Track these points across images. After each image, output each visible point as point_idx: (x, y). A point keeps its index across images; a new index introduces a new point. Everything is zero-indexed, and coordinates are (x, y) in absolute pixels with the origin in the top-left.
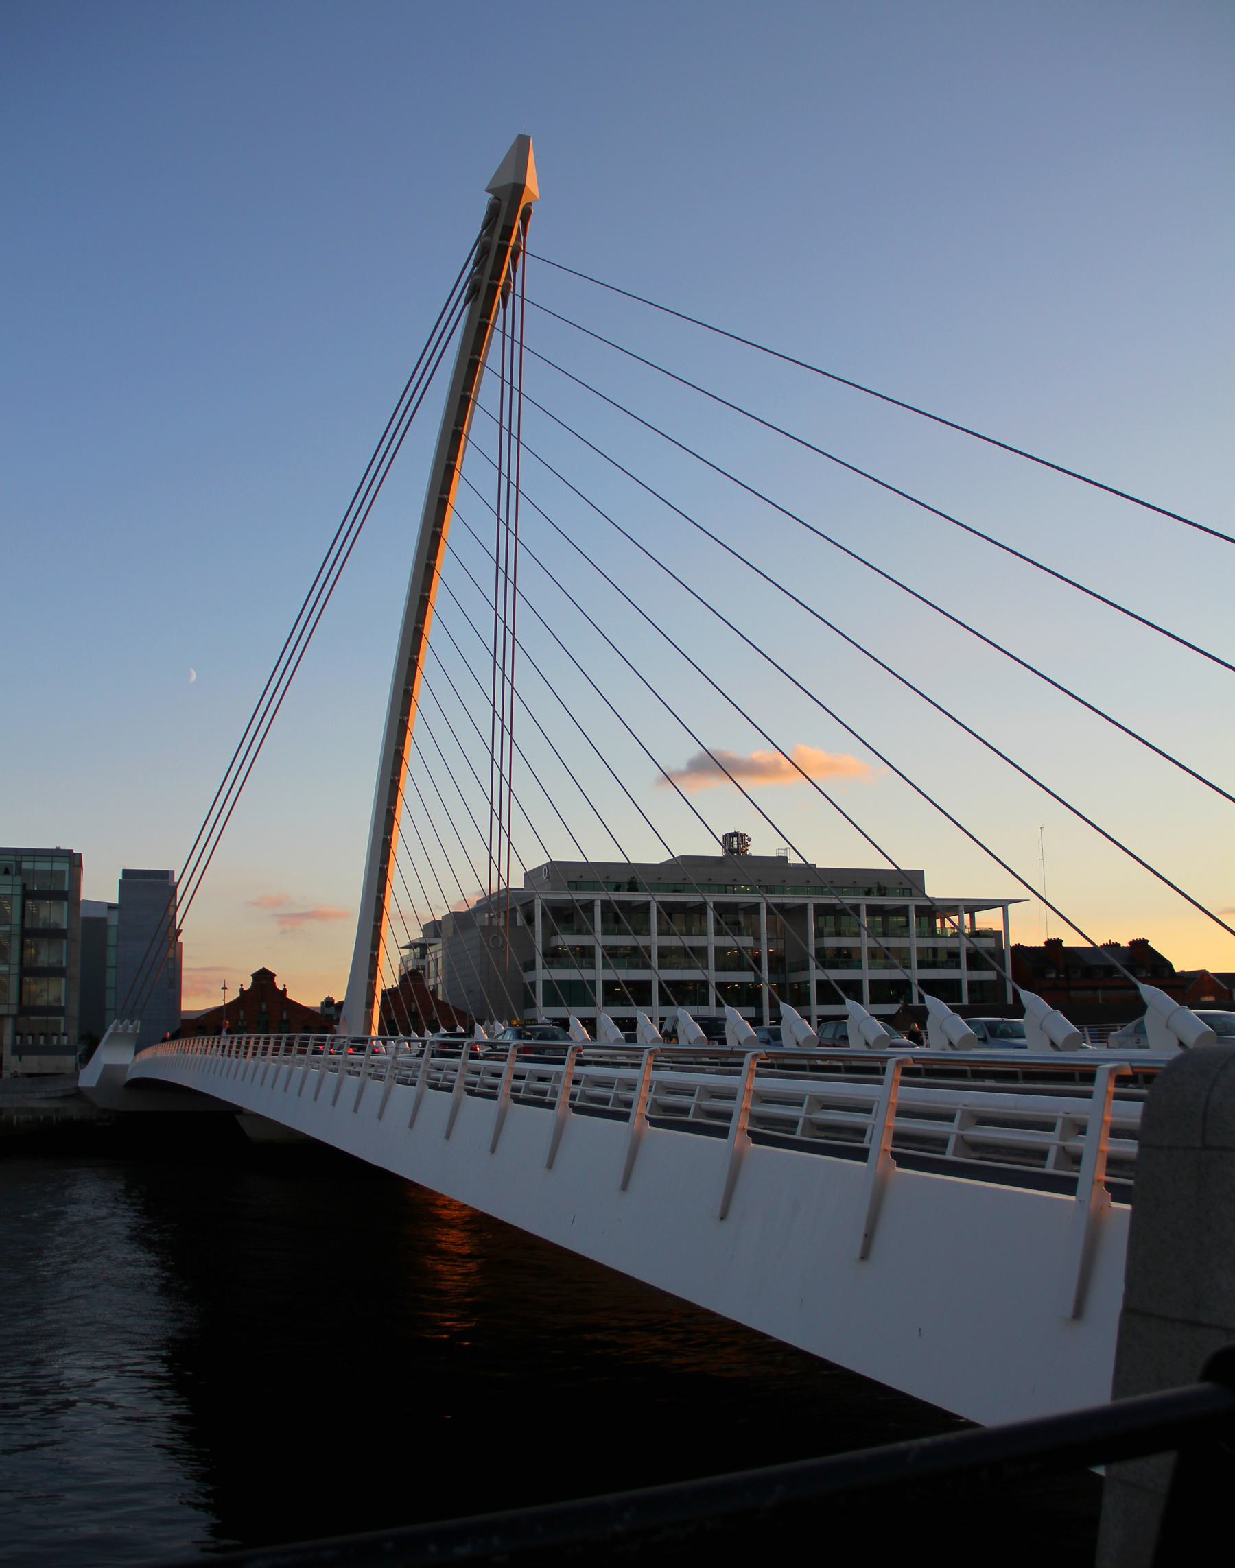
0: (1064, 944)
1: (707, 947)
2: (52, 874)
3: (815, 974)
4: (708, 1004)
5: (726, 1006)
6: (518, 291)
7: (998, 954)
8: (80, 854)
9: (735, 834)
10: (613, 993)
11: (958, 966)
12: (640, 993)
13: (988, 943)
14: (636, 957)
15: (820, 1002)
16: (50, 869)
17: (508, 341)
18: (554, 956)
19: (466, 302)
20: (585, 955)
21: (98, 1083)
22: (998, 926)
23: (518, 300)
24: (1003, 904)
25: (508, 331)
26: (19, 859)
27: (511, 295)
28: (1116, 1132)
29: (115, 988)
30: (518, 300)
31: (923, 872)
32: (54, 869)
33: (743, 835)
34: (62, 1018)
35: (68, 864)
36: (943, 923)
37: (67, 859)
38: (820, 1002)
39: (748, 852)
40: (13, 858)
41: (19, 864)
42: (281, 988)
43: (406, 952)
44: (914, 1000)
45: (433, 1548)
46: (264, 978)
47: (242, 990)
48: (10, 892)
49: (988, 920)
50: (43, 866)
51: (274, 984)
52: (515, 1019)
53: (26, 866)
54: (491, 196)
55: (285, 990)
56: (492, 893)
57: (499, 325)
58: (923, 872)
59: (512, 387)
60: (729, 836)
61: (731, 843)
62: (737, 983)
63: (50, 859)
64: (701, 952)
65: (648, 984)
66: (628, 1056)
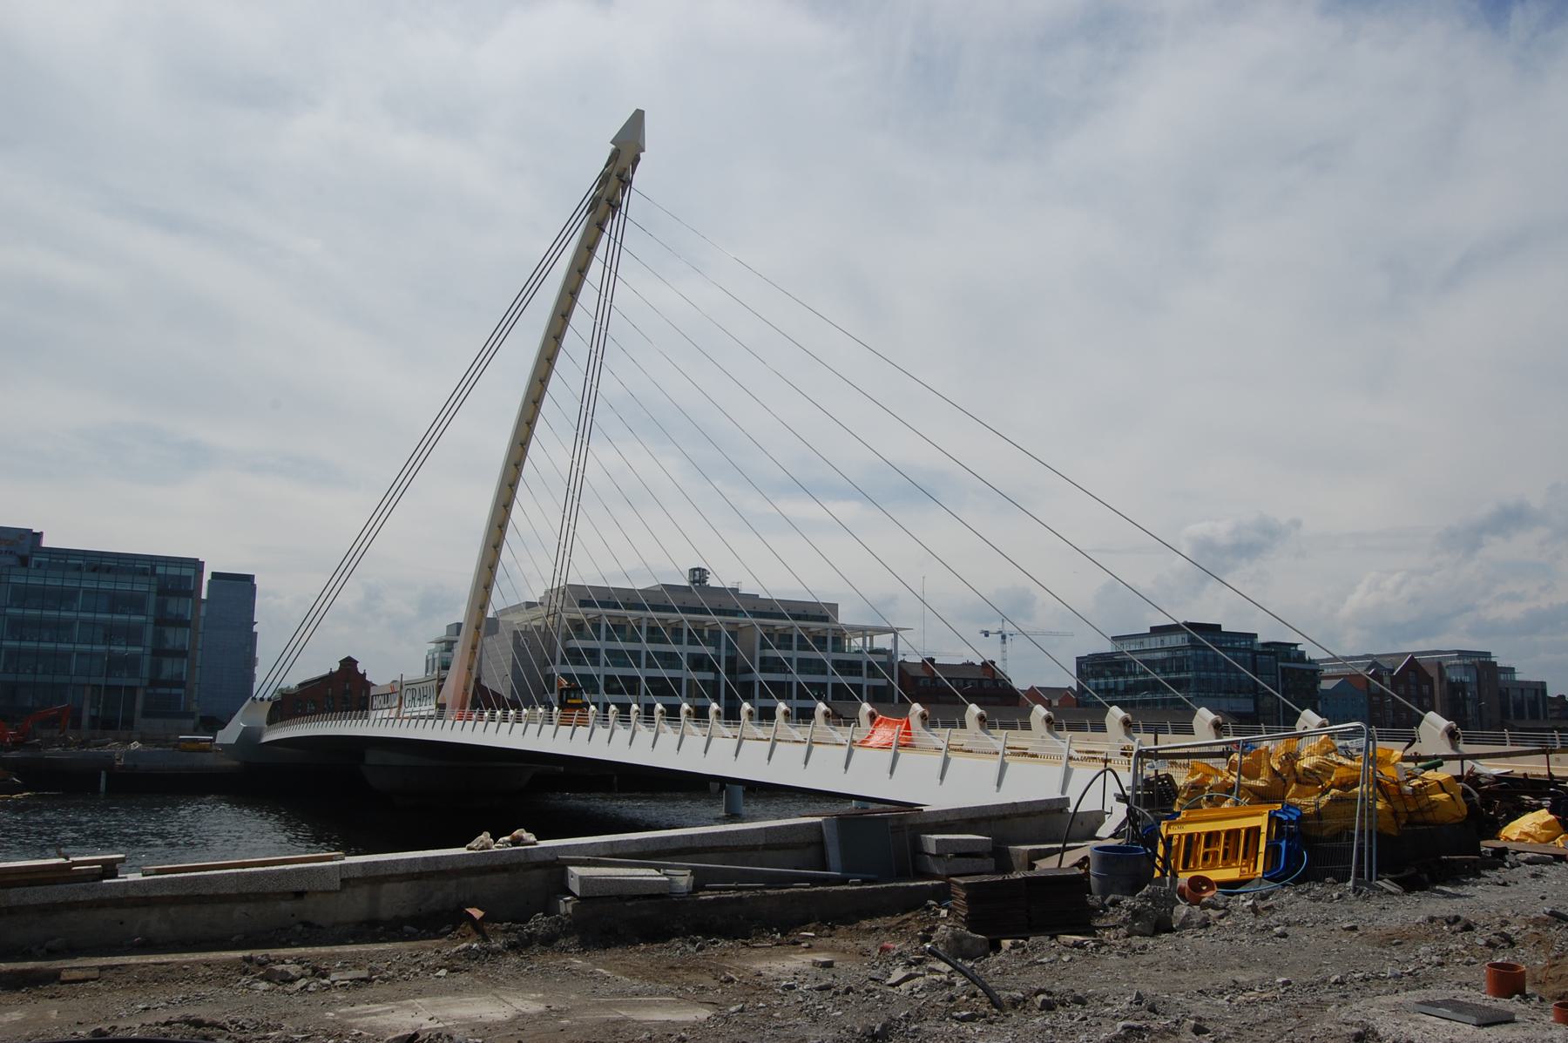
0: (46, 543)
2: (180, 578)
3: (759, 676)
5: (595, 674)
6: (623, 211)
7: (888, 667)
8: (203, 562)
9: (698, 569)
10: (611, 685)
11: (860, 674)
12: (632, 685)
14: (670, 660)
16: (164, 573)
17: (612, 241)
19: (587, 213)
20: (593, 654)
21: (927, 812)
23: (622, 217)
24: (895, 632)
25: (613, 235)
26: (154, 563)
27: (618, 213)
28: (1545, 913)
29: (200, 667)
30: (622, 217)
32: (168, 573)
33: (704, 570)
34: (181, 691)
36: (850, 642)
37: (194, 566)
39: (707, 583)
40: (149, 563)
42: (362, 672)
43: (433, 646)
44: (781, 680)
45: (1434, 725)
46: (349, 664)
47: (331, 672)
48: (147, 590)
49: (883, 642)
51: (357, 669)
53: (160, 570)
54: (613, 146)
55: (365, 674)
56: (1078, 811)
57: (607, 229)
59: (611, 269)
60: (693, 571)
61: (694, 575)
62: (1233, 867)
63: (165, 564)
64: (636, 655)
65: (824, 685)
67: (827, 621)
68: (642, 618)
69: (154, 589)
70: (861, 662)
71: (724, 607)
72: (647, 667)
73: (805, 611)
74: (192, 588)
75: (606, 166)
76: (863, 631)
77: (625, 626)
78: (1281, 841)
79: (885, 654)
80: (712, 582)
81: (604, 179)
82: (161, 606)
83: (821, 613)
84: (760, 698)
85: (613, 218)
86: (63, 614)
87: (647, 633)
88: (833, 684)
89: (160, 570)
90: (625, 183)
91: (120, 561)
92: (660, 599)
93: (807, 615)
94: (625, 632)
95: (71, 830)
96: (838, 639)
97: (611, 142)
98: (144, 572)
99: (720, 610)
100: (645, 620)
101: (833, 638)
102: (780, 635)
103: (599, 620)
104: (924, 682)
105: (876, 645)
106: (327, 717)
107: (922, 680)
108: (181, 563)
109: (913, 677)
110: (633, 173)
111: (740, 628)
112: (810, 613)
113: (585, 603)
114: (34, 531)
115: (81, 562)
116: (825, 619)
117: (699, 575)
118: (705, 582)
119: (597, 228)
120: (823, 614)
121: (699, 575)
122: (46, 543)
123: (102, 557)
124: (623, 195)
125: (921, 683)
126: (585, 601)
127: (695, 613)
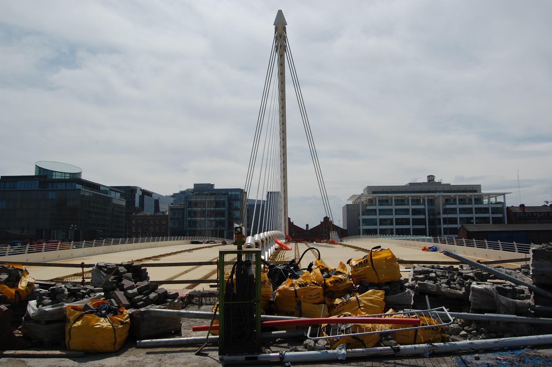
1: (409, 209)
4: (410, 225)
9: (430, 176)
13: (500, 206)
15: (444, 224)
18: (446, 211)
19: (276, 53)
22: (503, 201)
24: (504, 194)
26: (228, 191)
31: (1, 176)
33: (433, 176)
35: (239, 192)
38: (444, 224)
39: (435, 181)
41: (228, 193)
42: (292, 222)
47: (321, 222)
49: (500, 199)
50: (233, 193)
52: (62, 234)
55: (293, 222)
58: (1, 176)
63: (235, 191)
64: (455, 209)
66: (34, 250)
67: (476, 192)
68: (472, 195)
69: (227, 199)
70: (488, 208)
71: (452, 190)
72: (395, 215)
73: (466, 189)
74: (239, 198)
75: (275, 34)
76: (489, 195)
77: (465, 199)
78: (418, 285)
79: (501, 204)
80: (436, 180)
81: (276, 38)
82: (230, 204)
83: (475, 189)
84: (443, 224)
85: (286, 52)
86: (221, 209)
87: (475, 201)
88: (492, 218)
89: (230, 193)
90: (285, 38)
91: (218, 191)
92: (413, 188)
93: (466, 190)
94: (450, 201)
95: (502, 271)
96: (479, 200)
97: (274, 25)
98: (225, 194)
99: (383, 192)
100: (377, 197)
101: (411, 200)
102: (453, 199)
103: (455, 197)
104: (519, 214)
105: (498, 201)
106: (201, 238)
107: (519, 213)
108: (236, 190)
109: (514, 213)
110: (286, 34)
111: (436, 198)
112: (468, 189)
113: (374, 193)
114: (211, 184)
115: (207, 193)
116: (475, 191)
117: (431, 178)
118: (434, 180)
119: (282, 57)
120: (474, 189)
121: (431, 178)
122: (216, 187)
123: (231, 190)
124: (286, 43)
125: (518, 215)
126: (375, 192)
127: (419, 193)
